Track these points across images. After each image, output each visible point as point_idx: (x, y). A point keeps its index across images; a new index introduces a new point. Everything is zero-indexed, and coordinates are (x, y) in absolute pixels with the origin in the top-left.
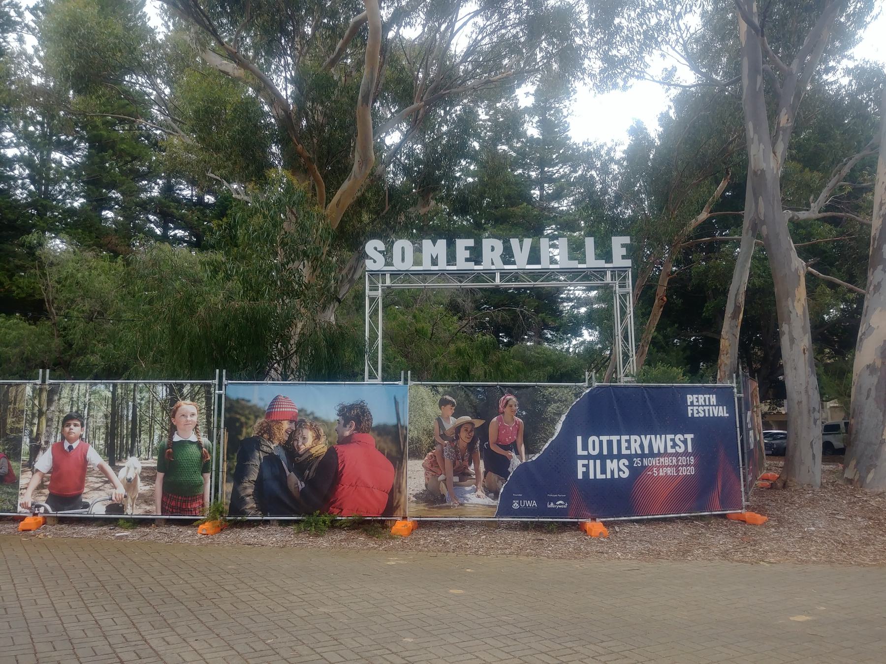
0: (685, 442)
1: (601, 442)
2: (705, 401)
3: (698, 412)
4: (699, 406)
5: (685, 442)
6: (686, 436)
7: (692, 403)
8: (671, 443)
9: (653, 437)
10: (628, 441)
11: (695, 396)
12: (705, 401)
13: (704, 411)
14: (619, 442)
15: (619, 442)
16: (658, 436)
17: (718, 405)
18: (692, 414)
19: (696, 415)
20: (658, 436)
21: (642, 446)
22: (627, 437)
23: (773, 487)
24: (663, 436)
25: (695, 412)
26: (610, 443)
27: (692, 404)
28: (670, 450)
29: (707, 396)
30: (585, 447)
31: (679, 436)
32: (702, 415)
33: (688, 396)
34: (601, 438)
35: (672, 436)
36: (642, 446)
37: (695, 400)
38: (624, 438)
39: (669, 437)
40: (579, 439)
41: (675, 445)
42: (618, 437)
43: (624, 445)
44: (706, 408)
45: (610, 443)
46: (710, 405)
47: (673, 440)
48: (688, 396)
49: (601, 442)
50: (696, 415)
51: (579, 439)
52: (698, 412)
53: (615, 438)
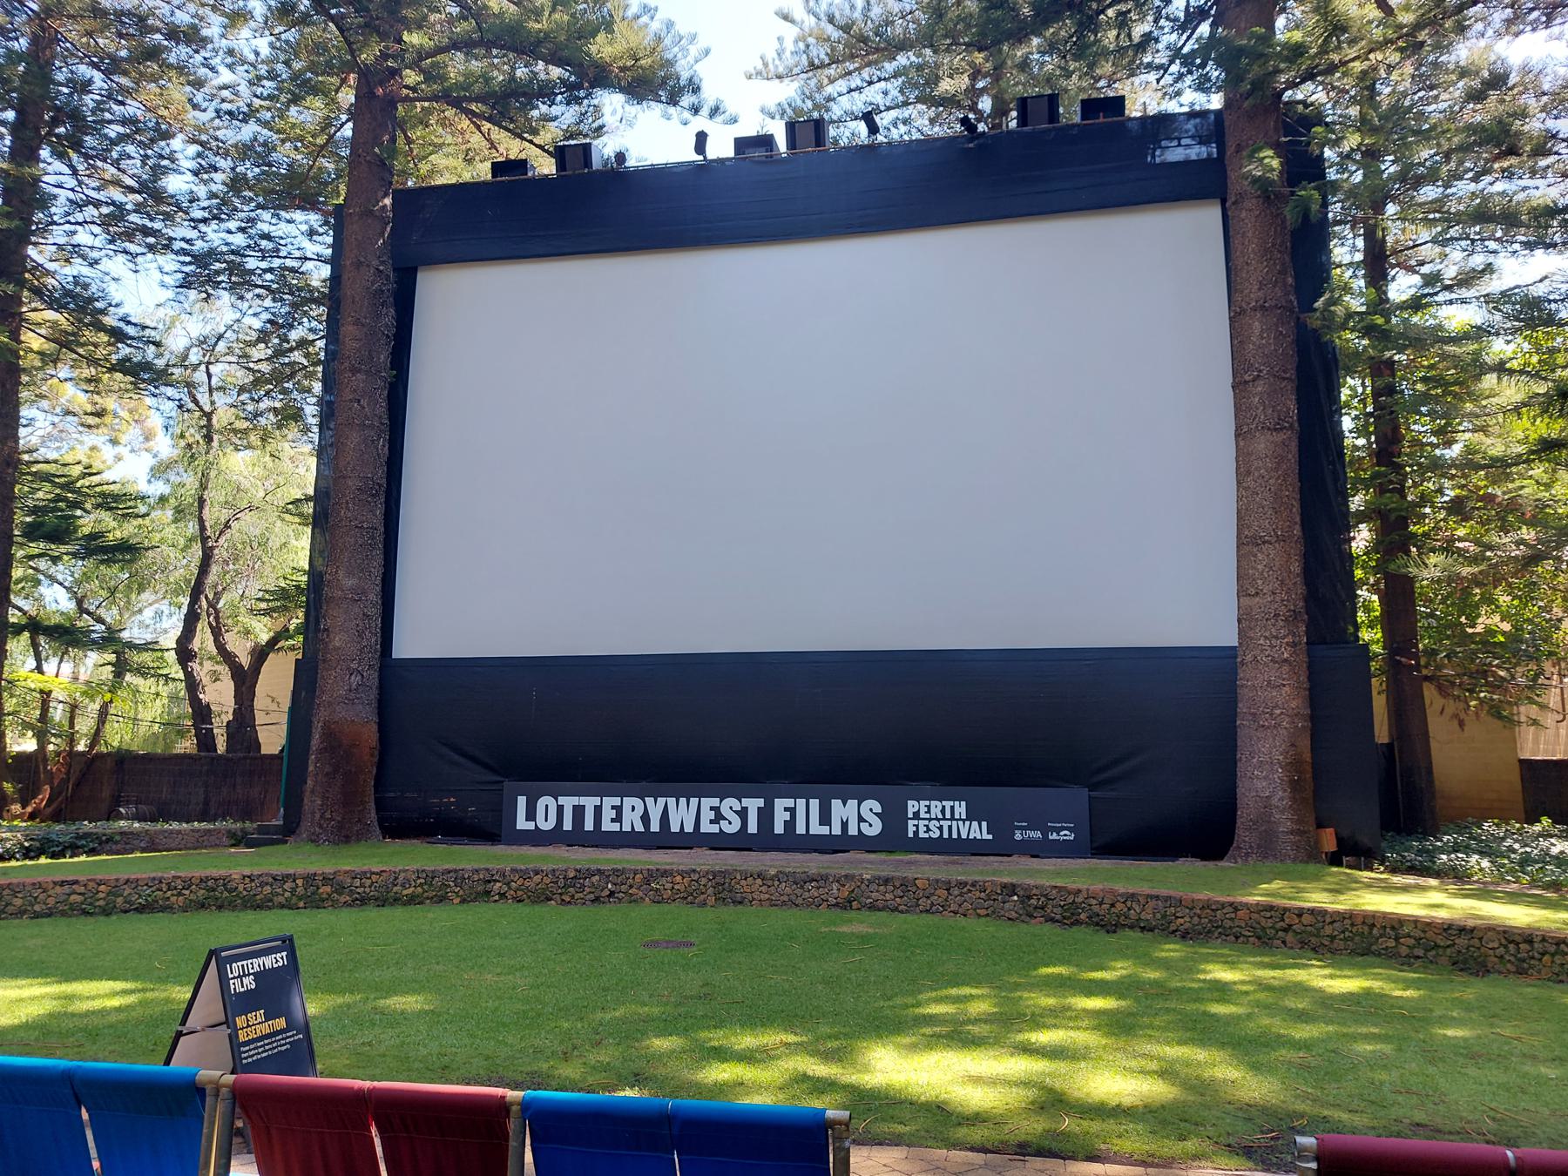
0: (743, 814)
1: (560, 809)
2: (943, 811)
3: (928, 830)
4: (930, 819)
5: (743, 814)
6: (746, 802)
7: (916, 815)
8: (712, 815)
9: (672, 801)
10: (618, 809)
11: (923, 803)
12: (943, 811)
13: (941, 828)
14: (598, 810)
15: (598, 810)
16: (683, 800)
17: (970, 818)
18: (916, 833)
19: (922, 835)
20: (683, 800)
21: (645, 818)
22: (616, 801)
23: (837, 905)
24: (694, 801)
25: (922, 829)
26: (579, 811)
27: (916, 815)
28: (707, 827)
29: (947, 804)
30: (531, 815)
31: (731, 802)
32: (935, 834)
33: (910, 803)
34: (562, 800)
35: (715, 802)
36: (645, 818)
37: (923, 810)
38: (609, 802)
39: (708, 802)
40: (522, 801)
41: (718, 817)
42: (597, 801)
43: (608, 814)
44: (945, 824)
45: (579, 811)
46: (952, 818)
47: (716, 809)
48: (910, 803)
49: (560, 809)
50: (922, 835)
51: (522, 801)
52: (928, 830)
53: (590, 802)
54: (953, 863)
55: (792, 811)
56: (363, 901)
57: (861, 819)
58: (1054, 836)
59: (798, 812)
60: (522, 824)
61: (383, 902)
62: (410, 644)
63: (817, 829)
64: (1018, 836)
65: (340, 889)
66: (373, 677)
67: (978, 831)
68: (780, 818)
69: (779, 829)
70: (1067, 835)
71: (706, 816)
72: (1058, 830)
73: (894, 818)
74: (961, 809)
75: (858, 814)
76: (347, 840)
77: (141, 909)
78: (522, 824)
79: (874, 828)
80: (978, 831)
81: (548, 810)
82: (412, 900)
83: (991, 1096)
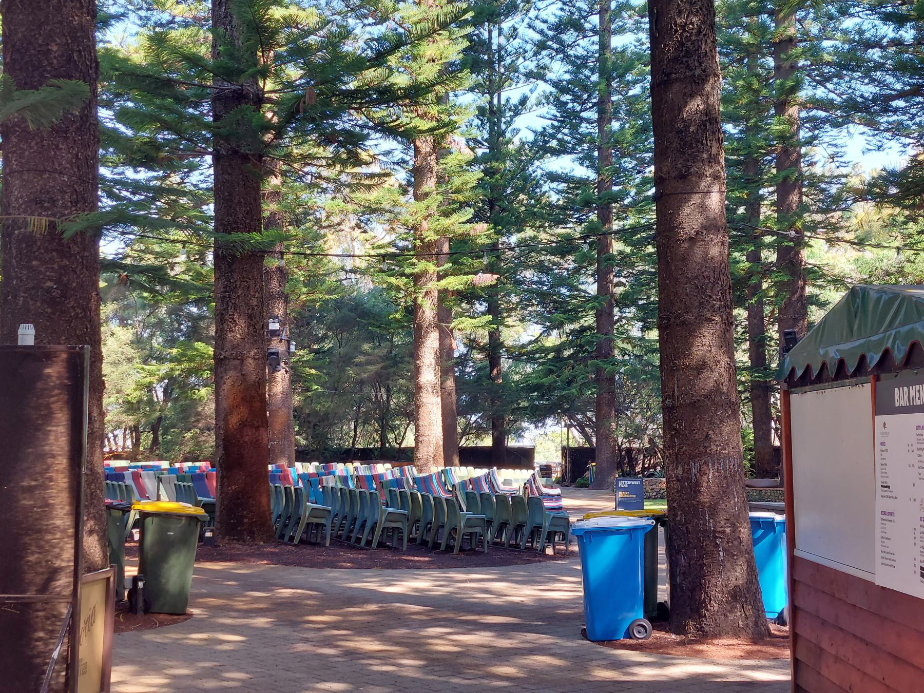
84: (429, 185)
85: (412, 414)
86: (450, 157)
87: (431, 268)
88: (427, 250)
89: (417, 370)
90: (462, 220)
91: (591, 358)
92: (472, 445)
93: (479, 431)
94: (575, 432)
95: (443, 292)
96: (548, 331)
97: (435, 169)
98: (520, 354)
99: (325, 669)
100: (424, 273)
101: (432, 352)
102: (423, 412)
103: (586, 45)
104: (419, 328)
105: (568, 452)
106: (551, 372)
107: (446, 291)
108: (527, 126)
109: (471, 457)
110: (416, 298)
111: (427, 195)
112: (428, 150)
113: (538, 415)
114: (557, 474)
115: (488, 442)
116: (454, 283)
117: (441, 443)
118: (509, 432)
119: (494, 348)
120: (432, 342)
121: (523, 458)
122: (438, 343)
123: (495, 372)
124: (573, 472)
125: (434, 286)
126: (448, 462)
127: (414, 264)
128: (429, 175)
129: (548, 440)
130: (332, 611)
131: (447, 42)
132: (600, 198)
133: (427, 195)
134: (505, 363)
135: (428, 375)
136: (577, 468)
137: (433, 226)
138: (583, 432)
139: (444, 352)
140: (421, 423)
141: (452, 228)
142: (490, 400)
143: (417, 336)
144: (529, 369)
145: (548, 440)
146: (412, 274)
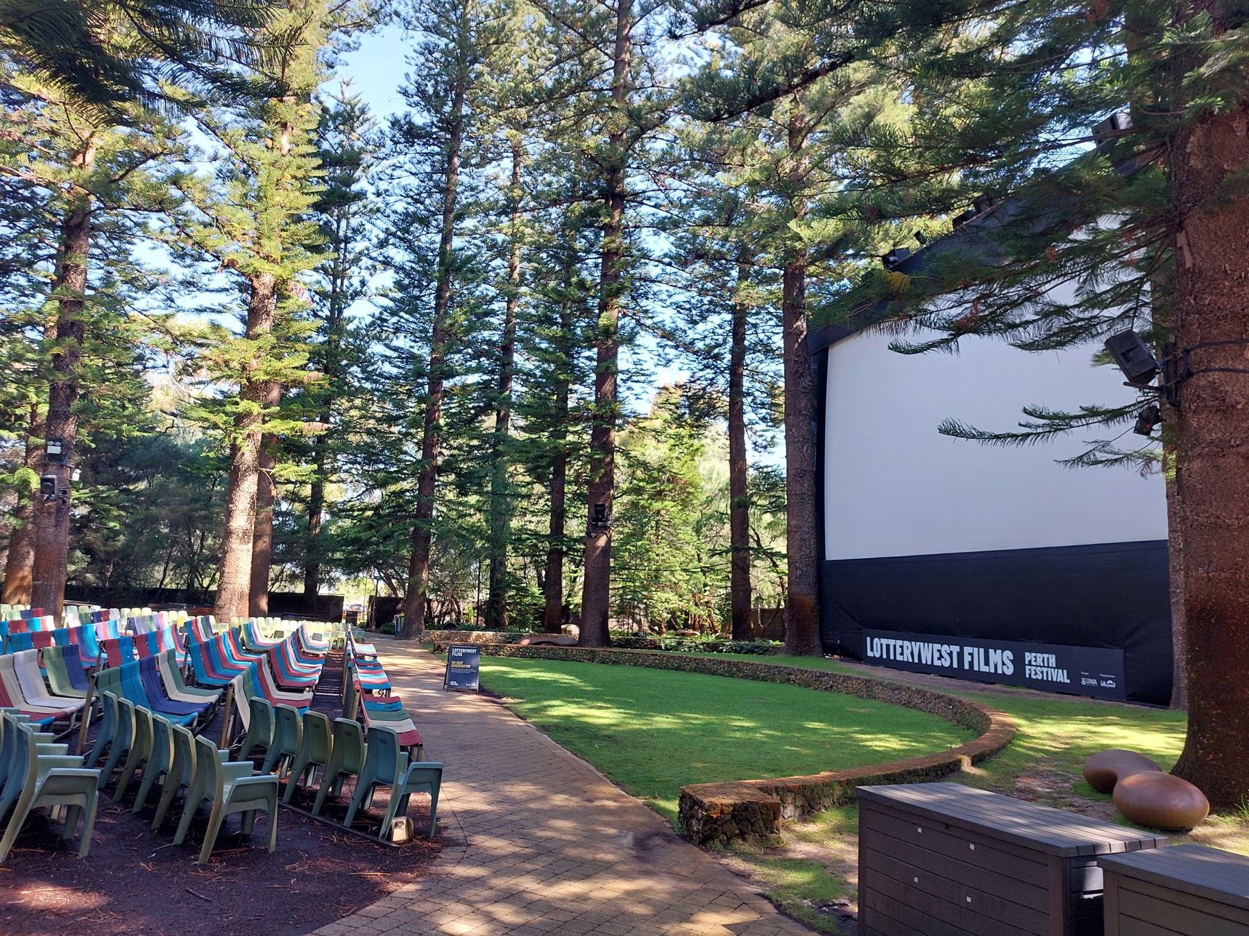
17: (1057, 667)
27: (1030, 664)
28: (937, 663)
29: (1046, 656)
44: (1045, 670)
54: (964, 687)
55: (971, 654)
56: (746, 677)
57: (1004, 664)
58: (1103, 684)
59: (974, 656)
60: (870, 654)
61: (755, 678)
62: (834, 552)
63: (984, 669)
64: (1083, 683)
65: (739, 670)
66: (811, 571)
67: (1061, 676)
68: (967, 659)
69: (967, 667)
70: (1110, 684)
71: (937, 655)
72: (1106, 680)
73: (1019, 663)
74: (1052, 660)
75: (1001, 660)
76: (800, 654)
77: (676, 669)
78: (870, 654)
79: (1009, 670)
80: (1061, 676)
81: (877, 646)
82: (763, 679)
83: (616, 716)
84: (264, 327)
85: (218, 559)
86: (291, 300)
87: (256, 408)
88: (252, 390)
89: (229, 514)
90: (297, 364)
91: (410, 517)
92: (286, 590)
93: (293, 578)
94: (382, 584)
95: (268, 439)
96: (370, 489)
97: (272, 313)
98: (338, 512)
99: (11, 568)
100: (248, 414)
101: (248, 496)
102: (231, 559)
103: (430, 238)
104: (237, 469)
105: (376, 601)
106: (371, 527)
107: (272, 435)
108: (360, 312)
109: (283, 606)
110: (235, 438)
111: (258, 336)
112: (266, 292)
113: (352, 567)
114: (362, 619)
115: (300, 588)
116: (280, 428)
117: (247, 591)
118: (322, 581)
119: (317, 498)
120: (249, 485)
121: (329, 610)
122: (256, 487)
123: (314, 521)
124: (377, 618)
125: (257, 428)
126: (254, 612)
127: (237, 403)
128: (264, 316)
129: (356, 592)
130: (1227, 861)
131: (297, 193)
132: (431, 372)
133: (258, 336)
134: (324, 517)
135: (241, 520)
136: (383, 618)
137: (264, 368)
138: (390, 585)
139: (263, 498)
140: (226, 570)
141: (283, 371)
142: (302, 554)
143: (234, 482)
144: (347, 523)
145: (356, 592)
146: (235, 413)
